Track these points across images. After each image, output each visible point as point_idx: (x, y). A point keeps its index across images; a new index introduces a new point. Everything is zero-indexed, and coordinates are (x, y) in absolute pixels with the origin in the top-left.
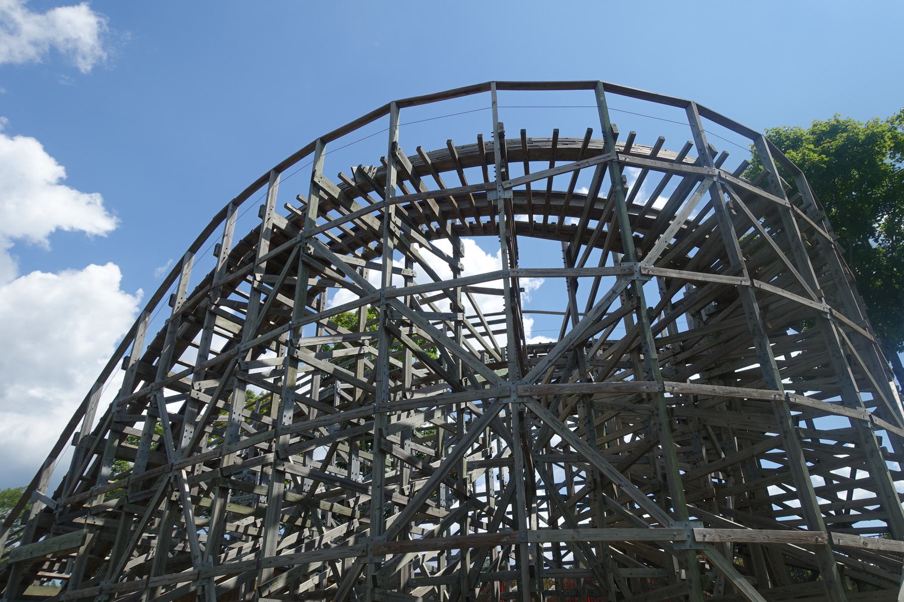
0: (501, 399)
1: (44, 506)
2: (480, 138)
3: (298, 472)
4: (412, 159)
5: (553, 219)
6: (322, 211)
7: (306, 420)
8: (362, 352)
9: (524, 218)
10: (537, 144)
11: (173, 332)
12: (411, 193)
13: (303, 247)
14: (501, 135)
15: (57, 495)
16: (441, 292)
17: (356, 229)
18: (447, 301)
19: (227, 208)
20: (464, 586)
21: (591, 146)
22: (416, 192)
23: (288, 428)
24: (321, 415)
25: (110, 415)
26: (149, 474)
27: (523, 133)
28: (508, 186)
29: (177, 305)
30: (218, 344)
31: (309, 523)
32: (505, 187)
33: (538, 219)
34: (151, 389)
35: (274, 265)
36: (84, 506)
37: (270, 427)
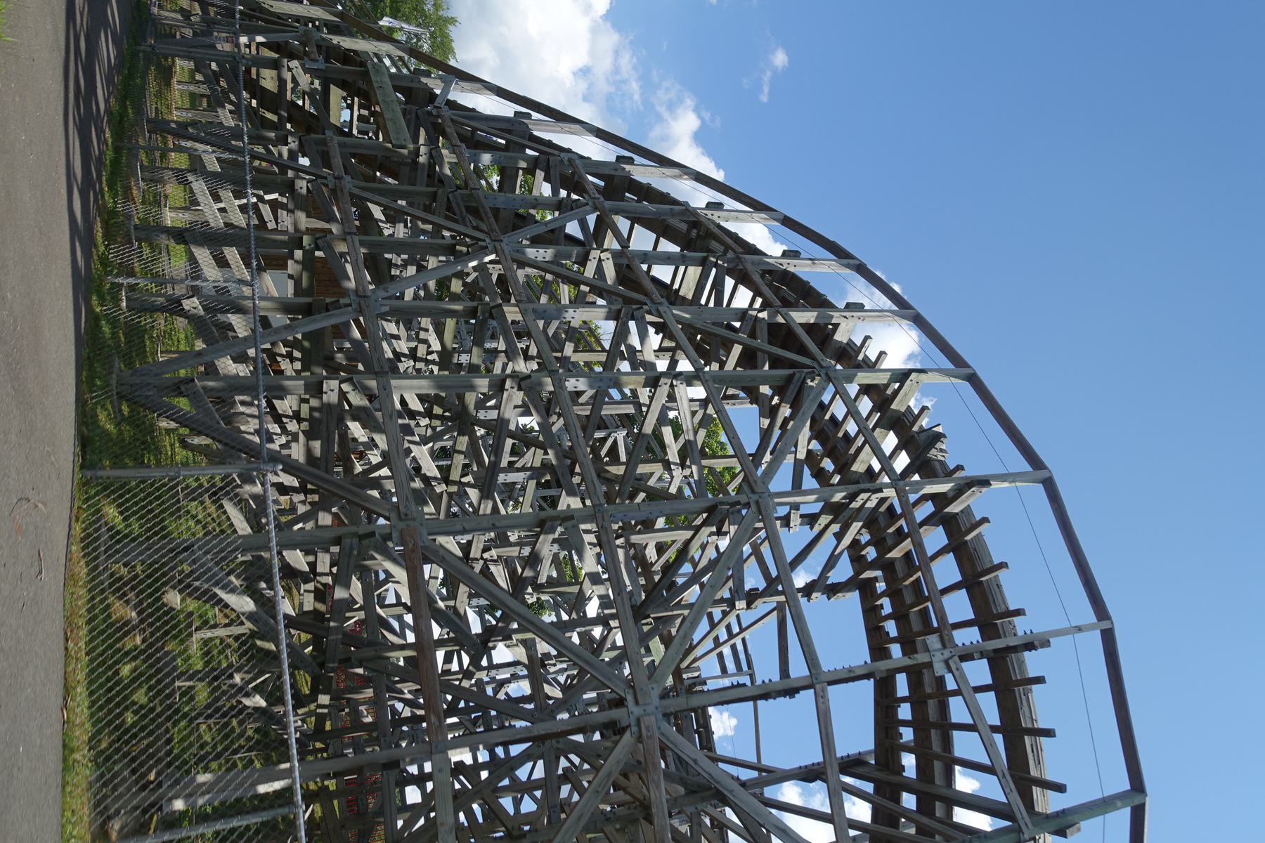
0: (631, 691)
1: (438, 92)
2: (1019, 612)
3: (505, 408)
4: (967, 511)
5: (907, 734)
6: (866, 389)
7: (573, 401)
8: (673, 467)
9: (902, 686)
10: (1025, 703)
11: (673, 214)
12: (860, 408)
13: (814, 372)
14: (1030, 646)
15: (453, 105)
16: (774, 573)
17: (848, 440)
18: (762, 585)
19: (852, 257)
20: (368, 652)
21: (1036, 791)
22: (918, 521)
23: (562, 387)
24: (580, 421)
25: (556, 152)
26: (486, 213)
27: (1039, 680)
28: (953, 667)
29: (709, 213)
30: (663, 273)
31: (436, 423)
32: (951, 662)
33: (905, 712)
34: (595, 198)
35: (783, 335)
36: (441, 138)
37: (559, 355)
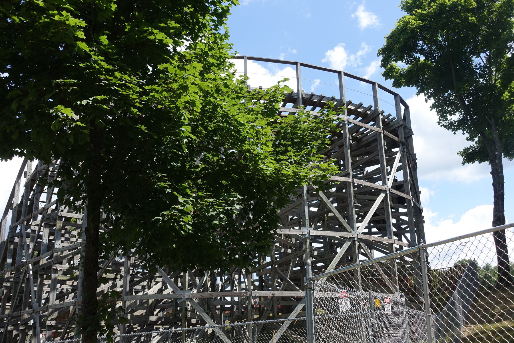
29: (27, 177)
